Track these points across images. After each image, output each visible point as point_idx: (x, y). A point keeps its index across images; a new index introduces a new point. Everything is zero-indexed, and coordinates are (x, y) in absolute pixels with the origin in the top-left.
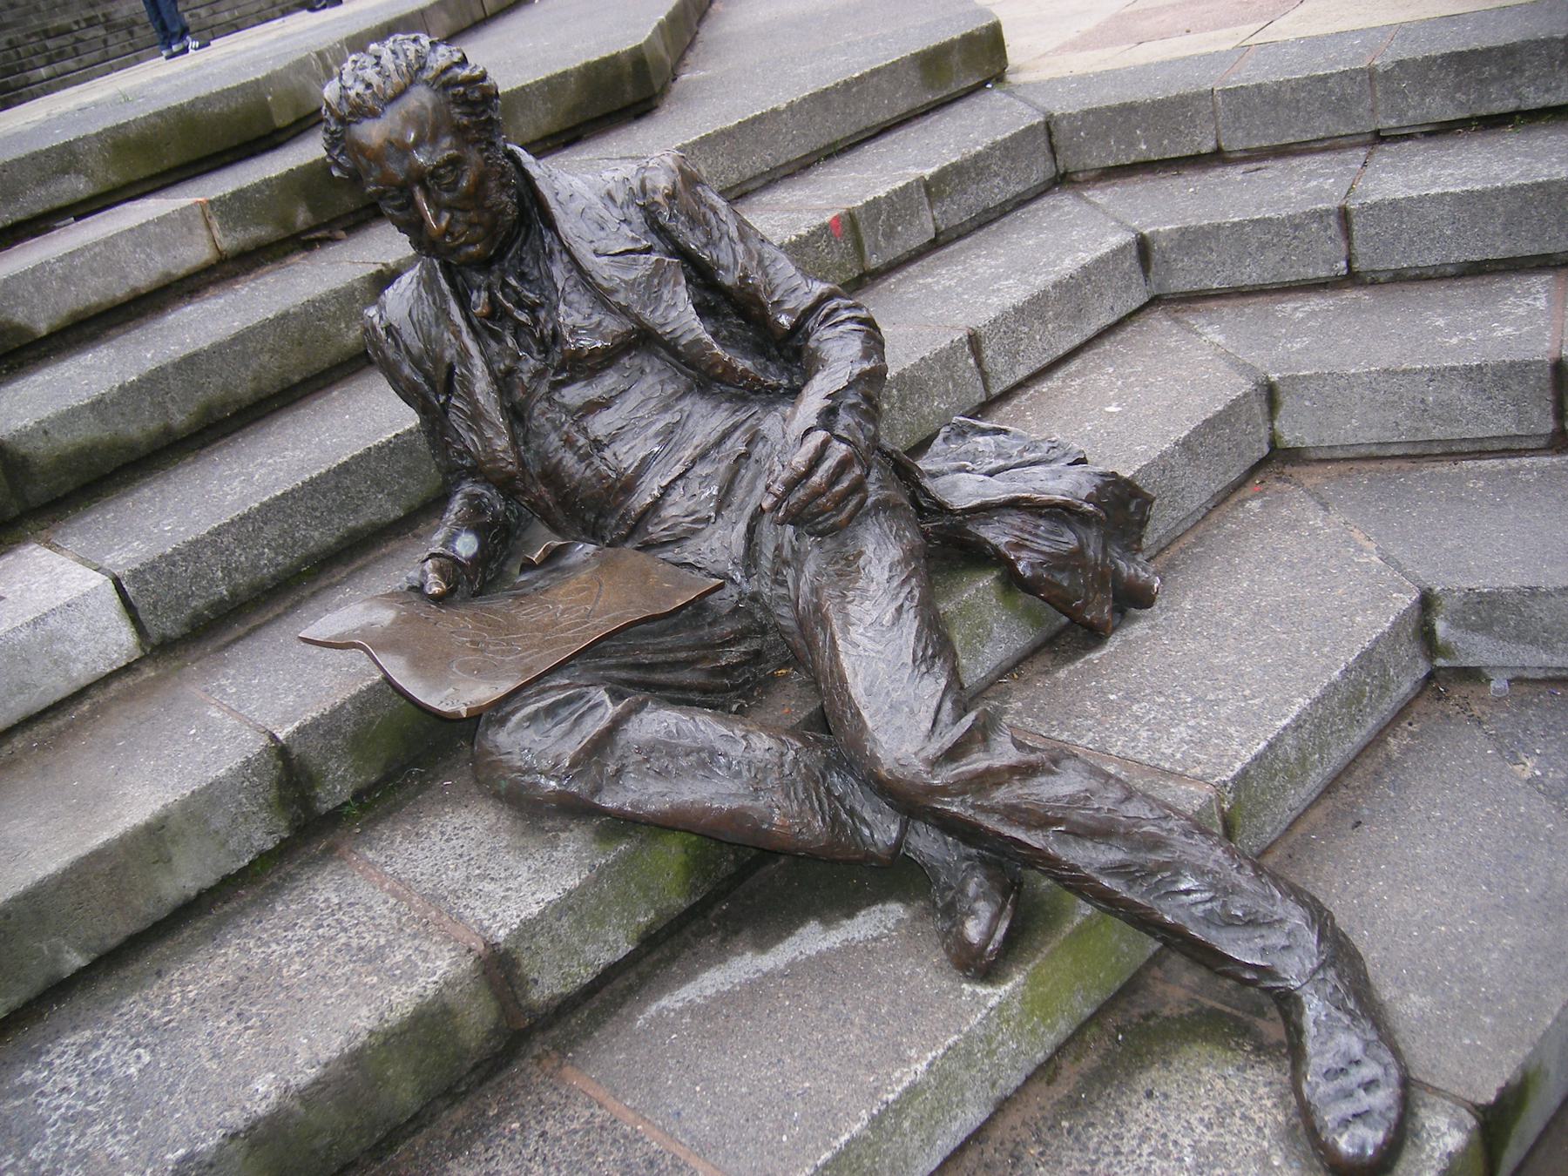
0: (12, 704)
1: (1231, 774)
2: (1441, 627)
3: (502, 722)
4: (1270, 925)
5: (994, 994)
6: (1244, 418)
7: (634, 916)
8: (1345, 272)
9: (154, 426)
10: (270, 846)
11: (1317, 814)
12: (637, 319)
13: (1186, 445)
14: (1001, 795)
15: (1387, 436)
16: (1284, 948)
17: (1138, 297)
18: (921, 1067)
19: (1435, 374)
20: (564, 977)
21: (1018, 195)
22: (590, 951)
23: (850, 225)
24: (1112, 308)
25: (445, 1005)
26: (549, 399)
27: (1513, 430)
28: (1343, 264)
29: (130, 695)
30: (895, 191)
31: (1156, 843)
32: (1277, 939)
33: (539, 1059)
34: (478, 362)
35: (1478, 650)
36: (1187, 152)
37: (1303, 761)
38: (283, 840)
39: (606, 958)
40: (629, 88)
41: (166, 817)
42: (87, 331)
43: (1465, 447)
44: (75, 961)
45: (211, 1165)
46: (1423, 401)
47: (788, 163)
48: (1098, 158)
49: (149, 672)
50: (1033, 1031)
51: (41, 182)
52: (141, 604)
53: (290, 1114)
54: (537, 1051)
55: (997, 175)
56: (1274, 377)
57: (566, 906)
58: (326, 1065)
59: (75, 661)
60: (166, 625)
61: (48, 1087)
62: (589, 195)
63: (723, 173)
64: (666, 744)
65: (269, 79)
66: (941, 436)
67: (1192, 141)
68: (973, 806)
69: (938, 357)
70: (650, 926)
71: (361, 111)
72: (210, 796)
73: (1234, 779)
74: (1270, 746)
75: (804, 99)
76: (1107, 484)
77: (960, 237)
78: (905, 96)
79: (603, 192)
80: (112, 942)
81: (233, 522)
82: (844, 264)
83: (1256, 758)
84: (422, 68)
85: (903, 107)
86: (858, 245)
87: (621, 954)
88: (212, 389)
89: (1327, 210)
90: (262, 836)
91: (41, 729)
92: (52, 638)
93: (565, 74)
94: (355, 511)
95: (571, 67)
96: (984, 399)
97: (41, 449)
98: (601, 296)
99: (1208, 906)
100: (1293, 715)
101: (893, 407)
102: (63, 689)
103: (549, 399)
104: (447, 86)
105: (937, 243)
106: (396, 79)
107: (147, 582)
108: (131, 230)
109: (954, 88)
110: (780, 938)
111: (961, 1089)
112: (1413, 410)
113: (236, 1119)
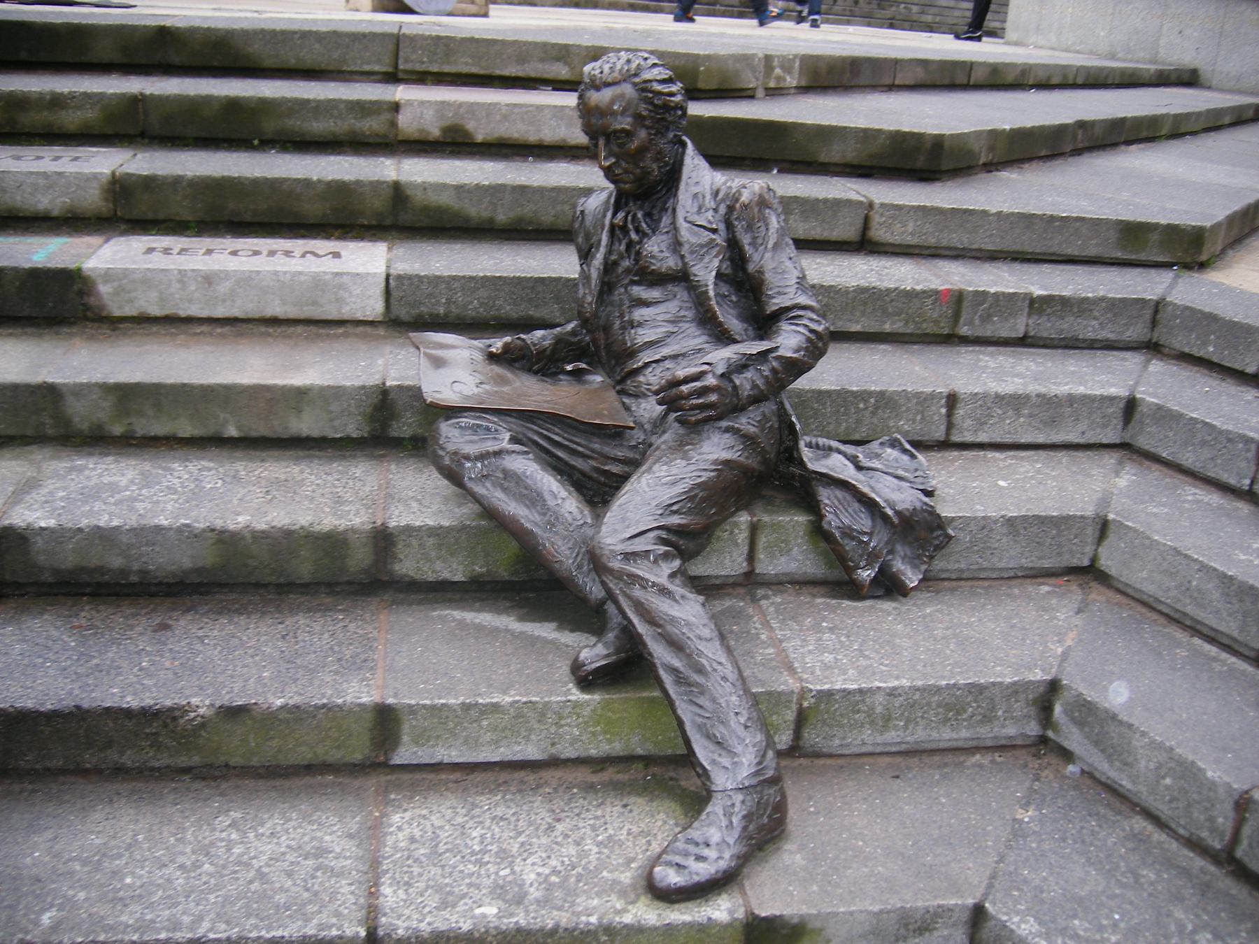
0: (305, 308)
1: (818, 687)
2: (1058, 709)
3: (448, 418)
4: (730, 752)
5: (576, 695)
6: (1074, 531)
7: (473, 564)
8: (1247, 488)
9: (485, 214)
10: (354, 436)
11: (887, 760)
12: (685, 264)
13: (1010, 522)
14: (637, 592)
15: (1159, 594)
16: (724, 767)
17: (1110, 436)
18: (508, 699)
19: (1204, 568)
20: (419, 569)
21: (1107, 340)
22: (439, 565)
23: (958, 299)
24: (1083, 433)
25: (346, 540)
26: (626, 288)
27: (1235, 634)
28: (1247, 482)
29: (364, 337)
30: (1003, 293)
31: (700, 670)
32: (726, 761)
33: (382, 600)
34: (602, 250)
35: (1072, 738)
36: (1237, 366)
37: (887, 719)
38: (362, 438)
39: (446, 575)
40: (922, 158)
41: (309, 390)
42: (505, 151)
43: (1205, 631)
44: (232, 432)
45: (196, 536)
46: (1189, 582)
47: (980, 250)
48: (1179, 342)
49: (381, 331)
50: (593, 734)
51: (542, 60)
52: (395, 294)
53: (243, 538)
54: (385, 598)
55: (1095, 318)
56: (1111, 516)
57: (434, 532)
58: (272, 527)
59: (347, 304)
60: (403, 313)
61: (176, 474)
62: (707, 187)
63: (925, 234)
64: (519, 477)
65: (708, 58)
66: (880, 440)
67: (1243, 360)
68: (621, 589)
69: (917, 395)
70: (482, 575)
71: (597, 85)
72: (336, 393)
73: (819, 692)
74: (861, 691)
75: (1012, 214)
76: (926, 511)
77: (1045, 346)
78: (1097, 245)
79: (715, 188)
80: (254, 434)
81: (464, 277)
82: (939, 322)
83: (844, 690)
84: (636, 75)
85: (1092, 251)
86: (957, 316)
87: (456, 579)
88: (527, 210)
89: (1252, 439)
90: (353, 428)
91: (314, 329)
92: (341, 286)
93: (879, 131)
94: (536, 307)
95: (885, 127)
96: (942, 439)
97: (418, 197)
98: (676, 245)
99: (705, 721)
100: (890, 685)
101: (866, 408)
102: (333, 315)
103: (626, 288)
104: (644, 90)
105: (1024, 342)
106: (616, 74)
107: (403, 285)
108: (555, 107)
109: (1143, 256)
110: (533, 621)
111: (531, 730)
112: (1181, 585)
113: (219, 524)
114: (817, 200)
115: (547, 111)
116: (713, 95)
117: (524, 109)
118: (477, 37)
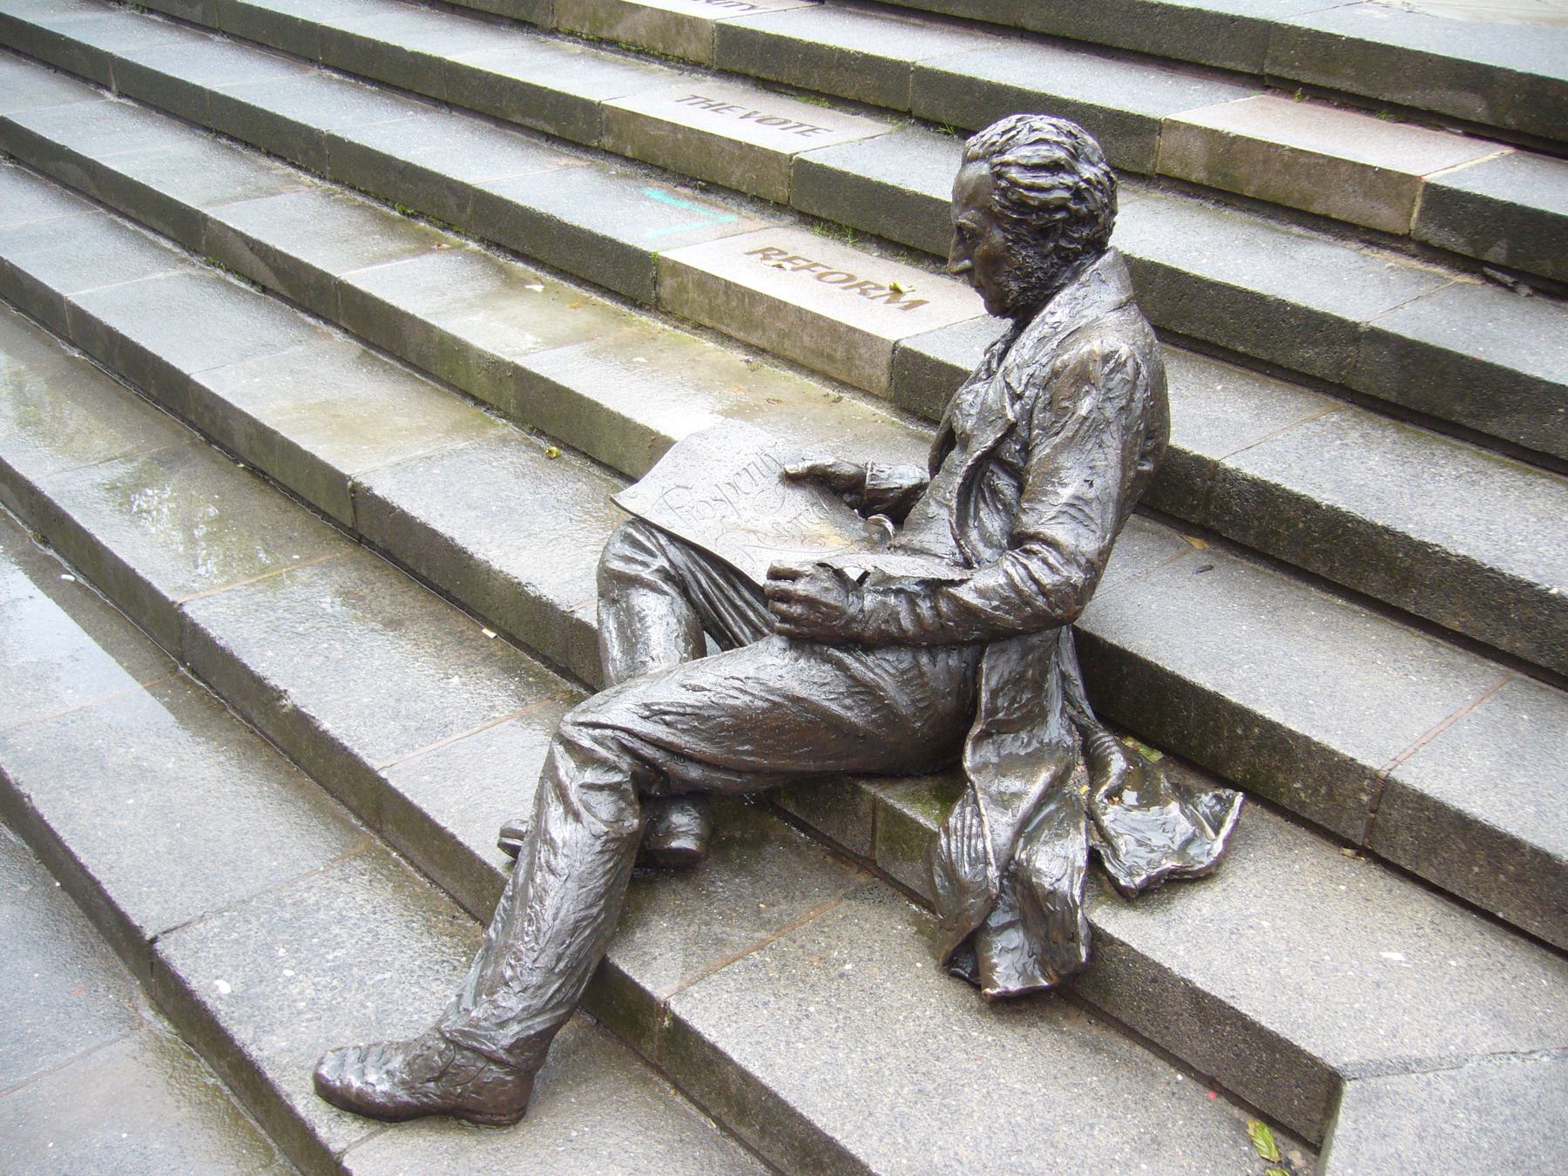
115: (1343, 169)
117: (1312, 160)
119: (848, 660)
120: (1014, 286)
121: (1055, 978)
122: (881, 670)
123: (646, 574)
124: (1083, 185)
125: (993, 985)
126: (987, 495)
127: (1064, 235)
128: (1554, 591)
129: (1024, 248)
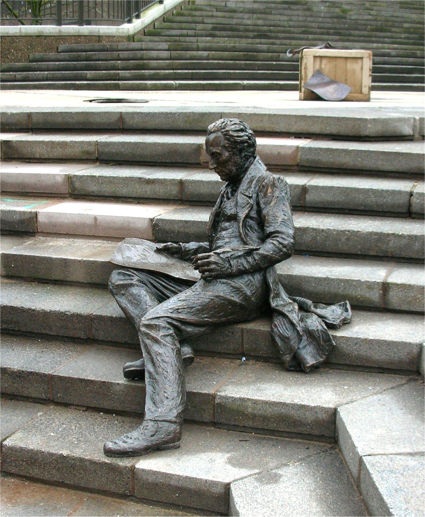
14: (148, 341)
57: (111, 319)
84: (224, 128)
114: (383, 190)
116: (381, 139)
118: (257, 113)
119: (229, 281)
120: (234, 168)
121: (324, 357)
122: (240, 283)
123: (133, 282)
124: (250, 135)
125: (308, 363)
126: (249, 229)
127: (246, 151)
128: (400, 234)
129: (236, 156)
